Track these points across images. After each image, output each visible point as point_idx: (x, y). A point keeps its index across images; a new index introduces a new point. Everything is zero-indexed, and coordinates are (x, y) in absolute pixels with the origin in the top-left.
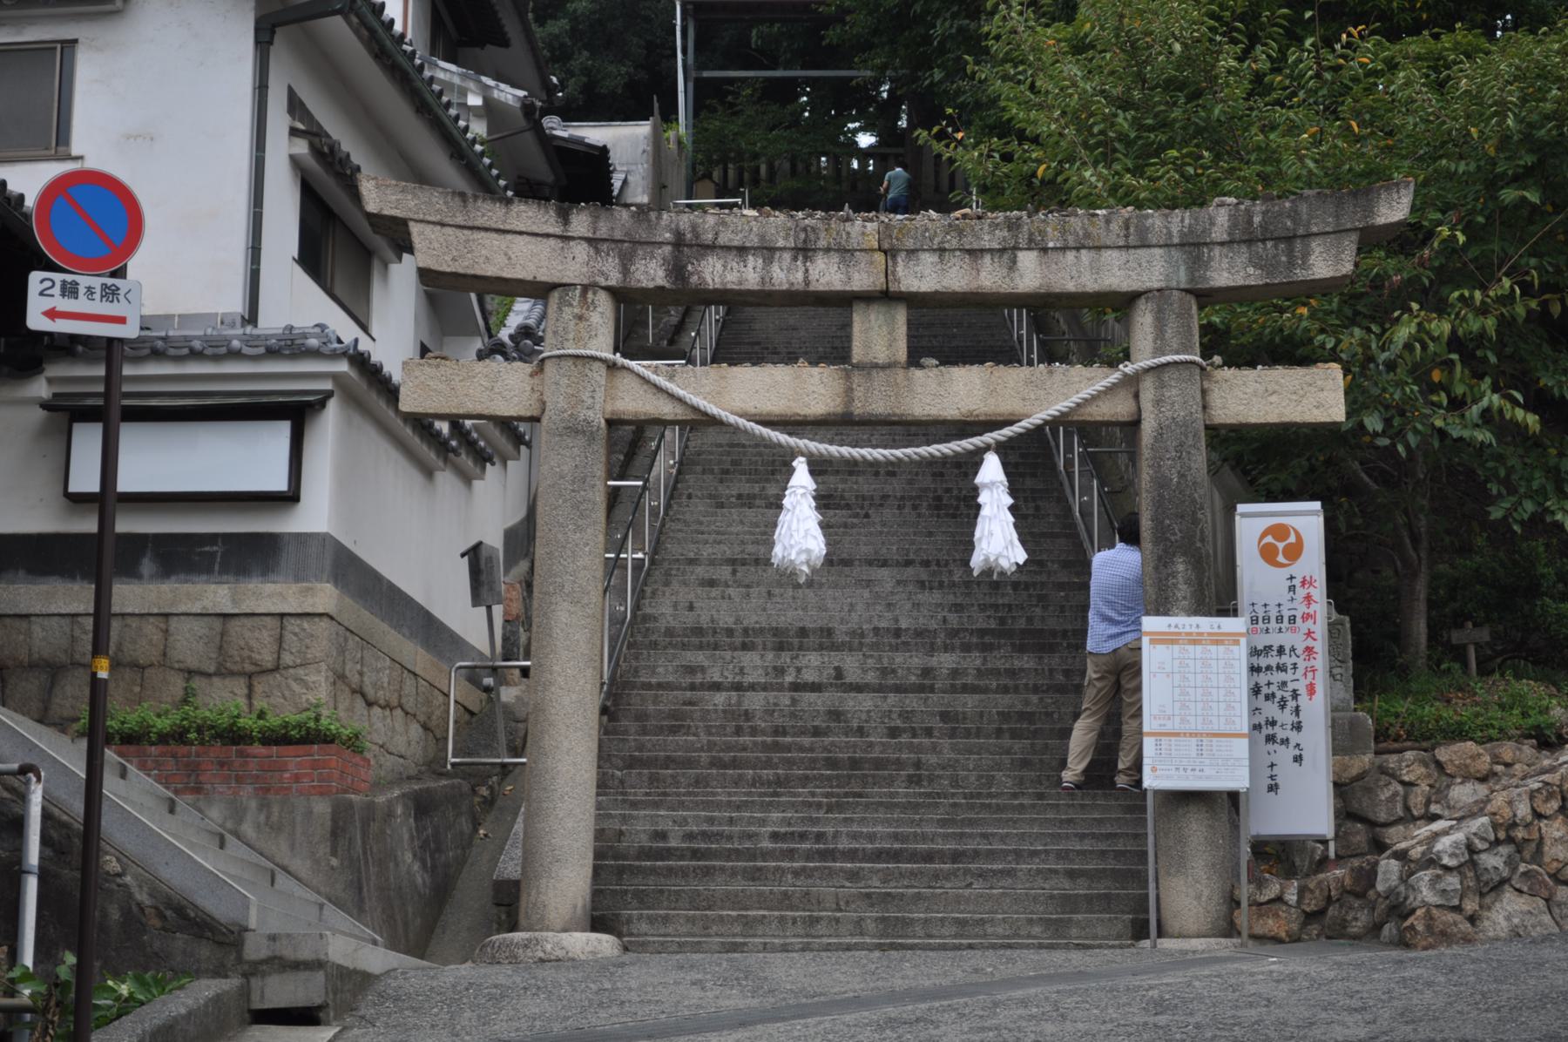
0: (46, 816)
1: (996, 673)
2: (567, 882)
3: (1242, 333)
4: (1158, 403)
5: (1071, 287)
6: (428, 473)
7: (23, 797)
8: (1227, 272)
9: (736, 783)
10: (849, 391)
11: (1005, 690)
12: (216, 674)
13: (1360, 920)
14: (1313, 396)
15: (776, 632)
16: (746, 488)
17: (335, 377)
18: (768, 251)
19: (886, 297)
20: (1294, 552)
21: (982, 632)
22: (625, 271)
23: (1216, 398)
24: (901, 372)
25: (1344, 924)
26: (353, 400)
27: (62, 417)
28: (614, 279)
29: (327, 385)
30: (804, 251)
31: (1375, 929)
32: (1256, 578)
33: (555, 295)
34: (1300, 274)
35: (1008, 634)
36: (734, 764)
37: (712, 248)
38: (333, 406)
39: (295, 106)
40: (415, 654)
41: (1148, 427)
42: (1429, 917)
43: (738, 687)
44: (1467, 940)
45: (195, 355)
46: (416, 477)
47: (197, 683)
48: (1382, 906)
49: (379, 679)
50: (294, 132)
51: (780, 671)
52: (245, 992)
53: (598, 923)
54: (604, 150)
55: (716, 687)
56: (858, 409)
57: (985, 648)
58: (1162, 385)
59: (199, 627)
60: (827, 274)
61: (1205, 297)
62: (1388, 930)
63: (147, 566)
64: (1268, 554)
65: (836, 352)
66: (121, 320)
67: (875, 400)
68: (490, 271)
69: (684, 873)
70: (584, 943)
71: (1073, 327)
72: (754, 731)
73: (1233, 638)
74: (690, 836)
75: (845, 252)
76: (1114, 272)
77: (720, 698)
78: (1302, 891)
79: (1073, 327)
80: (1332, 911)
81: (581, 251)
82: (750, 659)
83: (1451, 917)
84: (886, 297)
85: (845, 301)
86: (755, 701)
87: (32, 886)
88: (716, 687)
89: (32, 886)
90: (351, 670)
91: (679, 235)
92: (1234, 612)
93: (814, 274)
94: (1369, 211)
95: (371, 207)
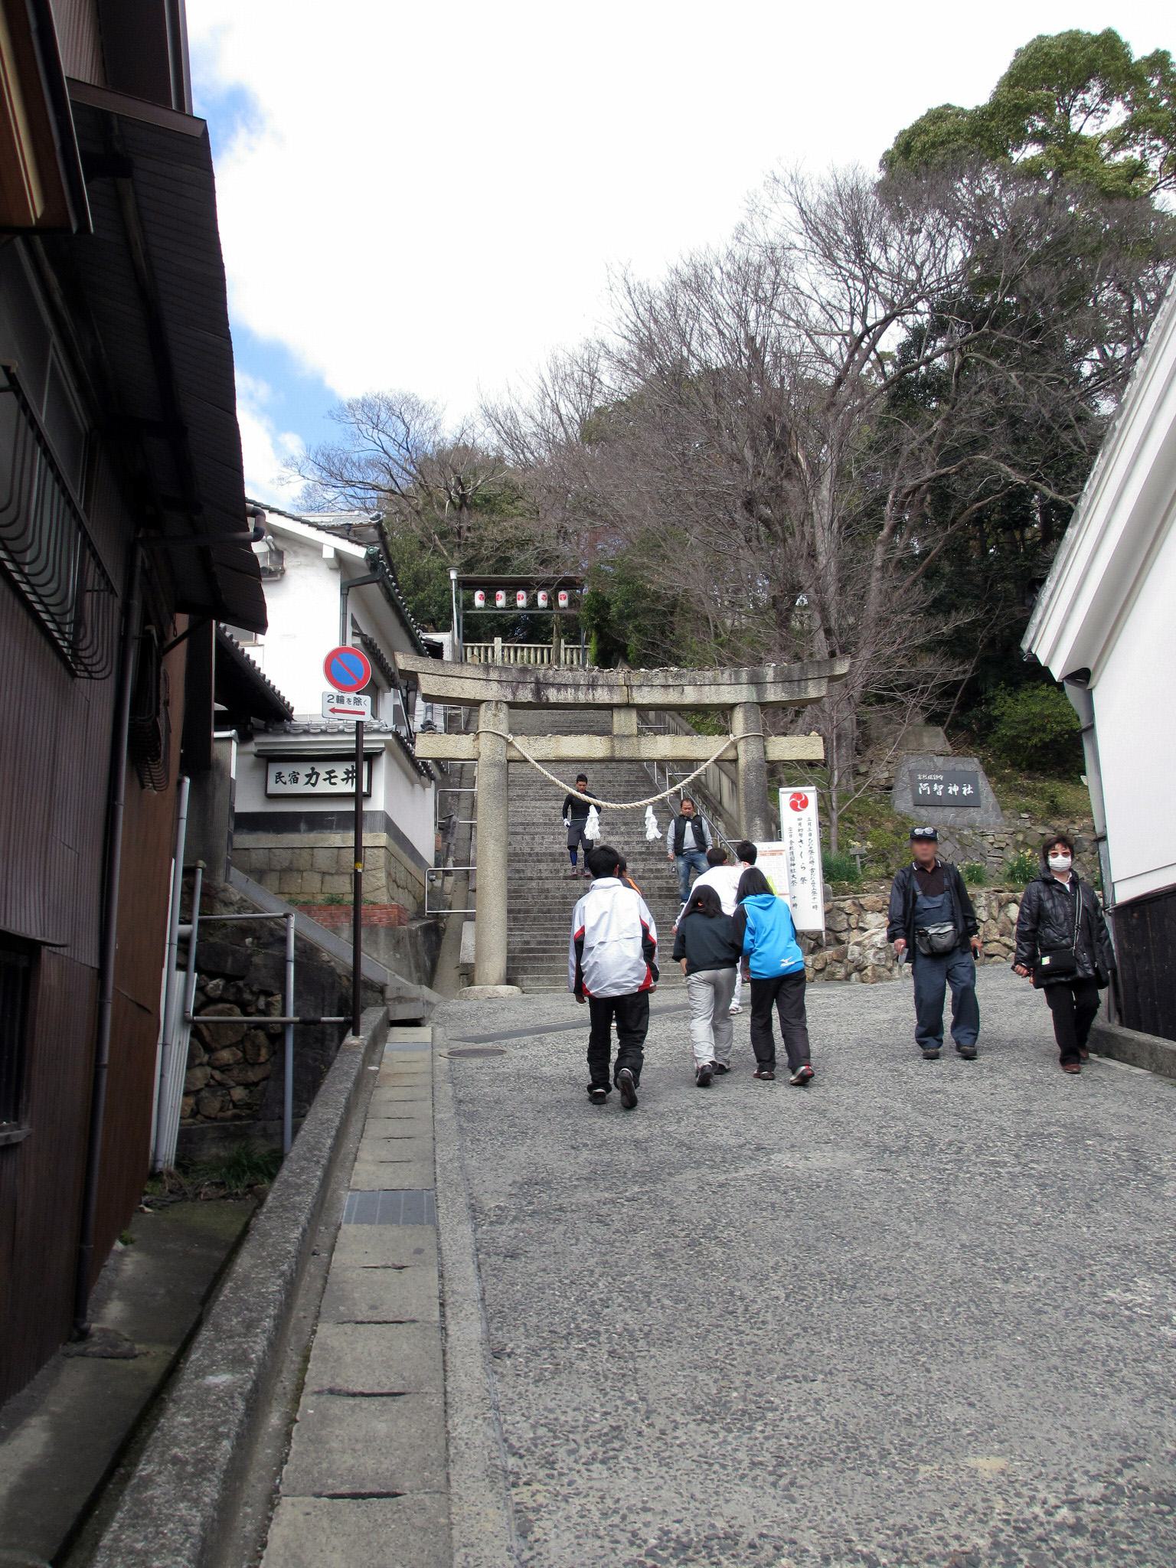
0: (296, 936)
1: (651, 870)
2: (495, 964)
3: (778, 717)
4: (746, 751)
5: (707, 701)
6: (413, 784)
7: (286, 929)
8: (773, 694)
9: (552, 920)
10: (613, 747)
11: (657, 878)
12: (337, 873)
13: (841, 972)
14: (807, 747)
15: (551, 854)
16: (520, 792)
17: (385, 741)
18: (577, 686)
19: (628, 706)
20: (805, 804)
21: (641, 853)
22: (514, 694)
23: (770, 749)
24: (635, 740)
25: (834, 974)
26: (392, 754)
27: (263, 761)
28: (510, 698)
29: (382, 746)
30: (592, 686)
31: (847, 977)
32: (788, 817)
33: (484, 705)
34: (804, 696)
35: (652, 854)
36: (549, 911)
37: (553, 685)
38: (384, 757)
39: (354, 623)
40: (411, 865)
41: (742, 762)
42: (873, 970)
43: (540, 878)
44: (889, 979)
45: (324, 732)
46: (408, 784)
47: (327, 878)
48: (851, 966)
49: (401, 876)
50: (354, 634)
51: (557, 871)
52: (387, 1013)
53: (509, 982)
54: (441, 644)
55: (531, 879)
56: (617, 754)
57: (644, 860)
58: (747, 744)
59: (327, 852)
60: (602, 696)
61: (764, 705)
62: (855, 976)
63: (303, 826)
64: (794, 806)
65: (605, 732)
66: (363, 713)
67: (625, 751)
68: (455, 695)
69: (541, 959)
70: (505, 990)
71: (709, 718)
72: (554, 897)
73: (780, 852)
74: (540, 943)
75: (611, 687)
76: (726, 695)
77: (534, 884)
78: (814, 960)
79: (709, 718)
80: (828, 969)
81: (495, 686)
82: (543, 866)
83: (882, 969)
84: (628, 706)
85: (610, 707)
86: (549, 885)
87: (292, 967)
88: (531, 879)
89: (292, 967)
90: (393, 871)
91: (537, 679)
92: (779, 839)
93: (597, 696)
94: (832, 669)
95: (401, 667)
